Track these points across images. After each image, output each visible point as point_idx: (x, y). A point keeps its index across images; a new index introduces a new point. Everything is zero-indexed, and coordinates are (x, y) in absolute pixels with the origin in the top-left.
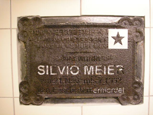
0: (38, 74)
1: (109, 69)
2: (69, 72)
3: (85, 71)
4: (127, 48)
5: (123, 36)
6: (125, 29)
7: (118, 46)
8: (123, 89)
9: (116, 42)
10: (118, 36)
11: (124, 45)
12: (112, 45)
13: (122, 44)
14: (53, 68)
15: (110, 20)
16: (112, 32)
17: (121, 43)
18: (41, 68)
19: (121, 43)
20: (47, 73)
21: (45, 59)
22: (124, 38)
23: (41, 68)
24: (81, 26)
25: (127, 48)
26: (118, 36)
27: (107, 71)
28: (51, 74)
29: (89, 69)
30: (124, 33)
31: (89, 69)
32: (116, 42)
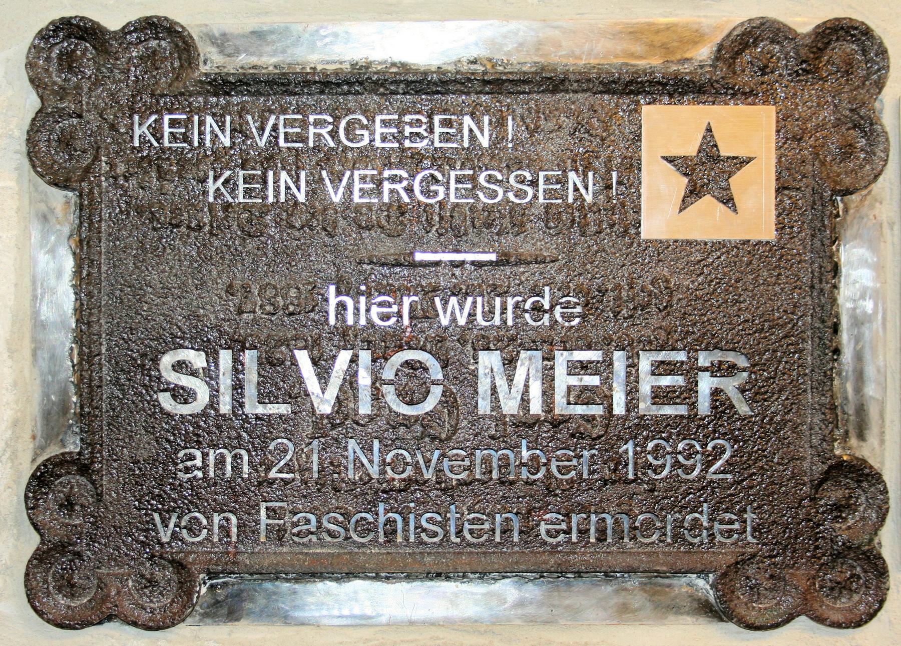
0: (156, 404)
1: (379, 130)
2: (377, 396)
3: (484, 386)
4: (769, 234)
5: (702, 132)
6: (760, 109)
7: (708, 222)
8: (749, 516)
9: (694, 192)
10: (709, 152)
11: (753, 212)
12: (663, 213)
13: (666, 159)
14: (267, 362)
15: (652, 46)
16: (669, 129)
17: (728, 201)
18: (180, 366)
19: (728, 201)
20: (225, 407)
21: (215, 308)
22: (746, 169)
23: (180, 366)
24: (459, 86)
25: (769, 234)
26: (709, 152)
27: (632, 392)
28: (253, 408)
29: (453, 313)
30: (749, 130)
31: (453, 313)
32: (694, 192)
